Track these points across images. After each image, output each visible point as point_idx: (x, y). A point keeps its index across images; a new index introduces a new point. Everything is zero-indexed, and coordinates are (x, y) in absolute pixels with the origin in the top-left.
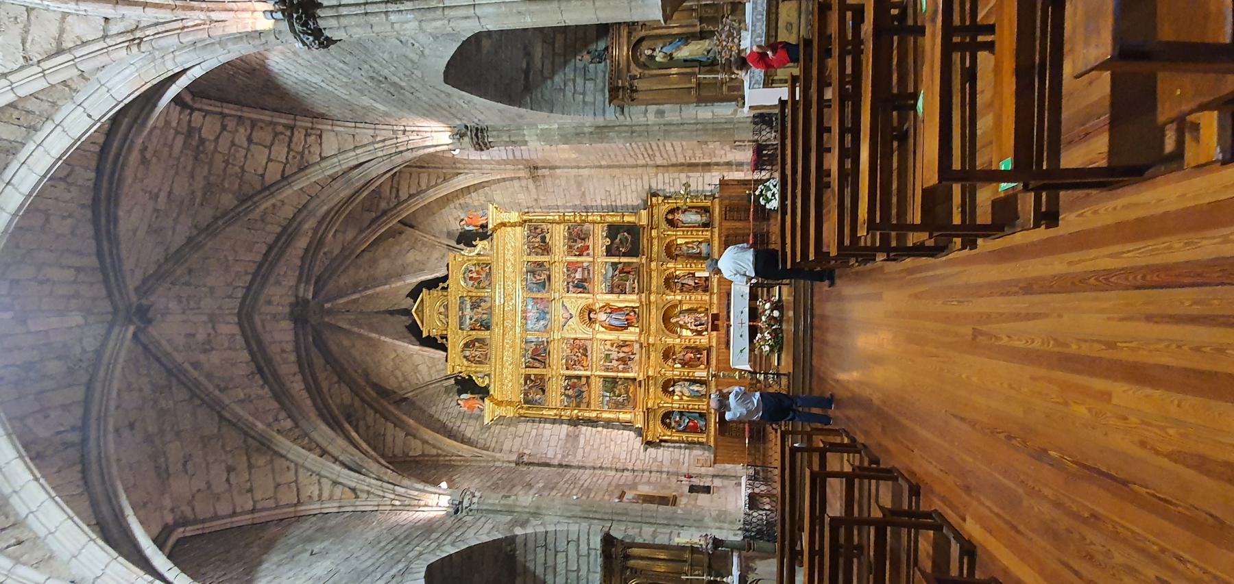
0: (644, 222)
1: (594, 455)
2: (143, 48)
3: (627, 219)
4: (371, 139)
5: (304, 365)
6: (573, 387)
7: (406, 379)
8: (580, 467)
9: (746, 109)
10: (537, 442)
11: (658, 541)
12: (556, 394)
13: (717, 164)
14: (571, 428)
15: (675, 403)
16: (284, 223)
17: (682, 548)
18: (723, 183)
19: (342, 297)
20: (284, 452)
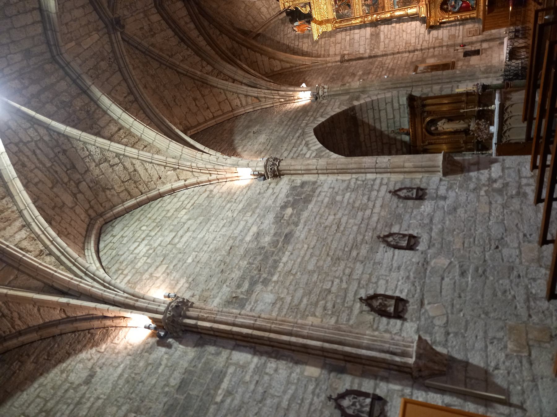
1: (392, 45)
5: (199, 28)
7: (256, 21)
8: (383, 56)
10: (351, 44)
11: (444, 93)
14: (373, 29)
17: (461, 94)
20: (215, 85)
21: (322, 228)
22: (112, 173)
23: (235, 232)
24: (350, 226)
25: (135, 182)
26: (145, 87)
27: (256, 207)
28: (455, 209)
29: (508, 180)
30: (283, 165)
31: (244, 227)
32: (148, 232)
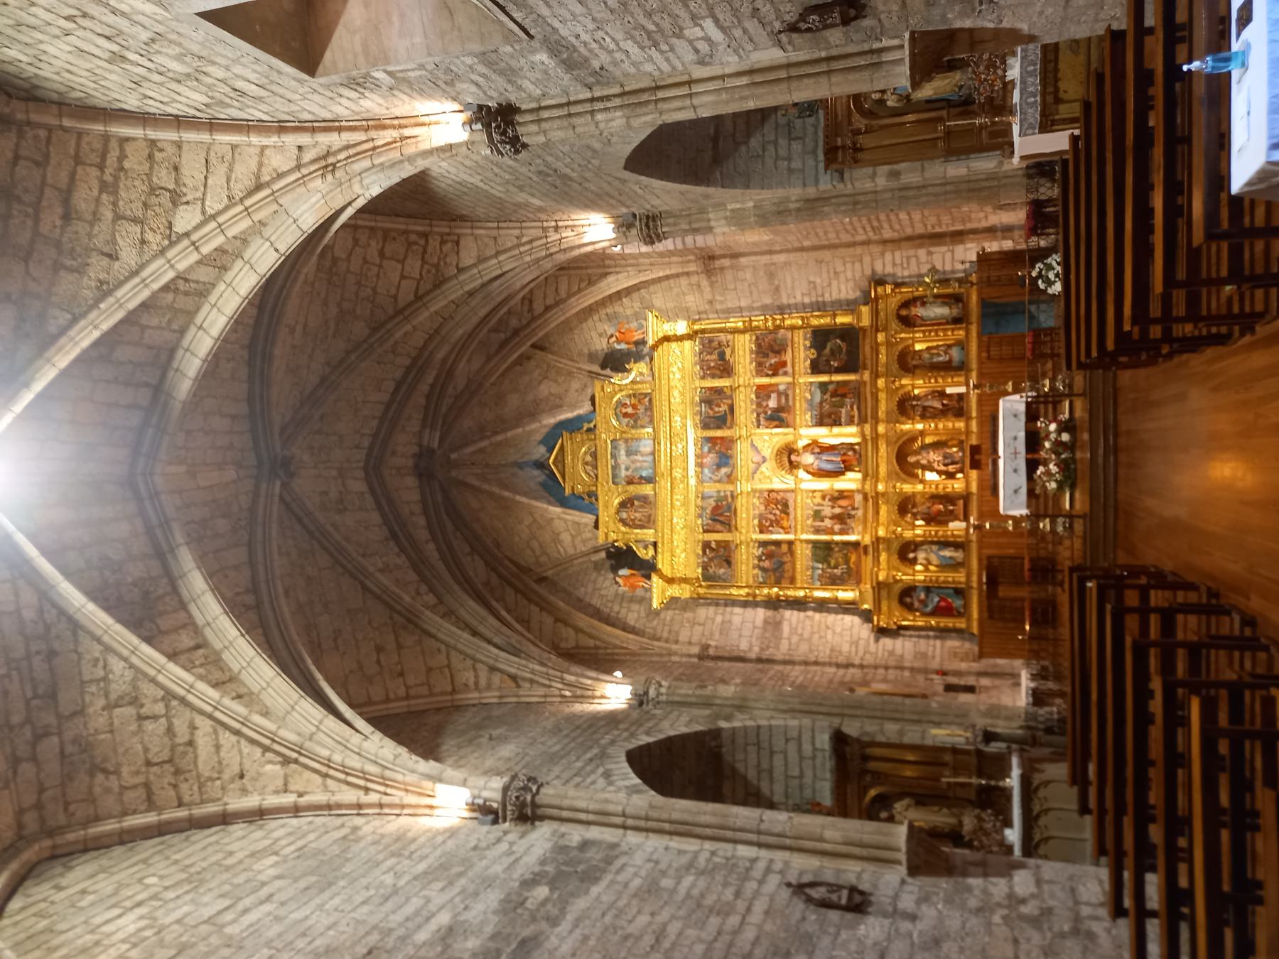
0: (866, 322)
2: (338, 174)
3: (839, 320)
4: (515, 241)
6: (770, 556)
7: (544, 553)
8: (785, 662)
9: (1016, 160)
11: (907, 740)
12: (746, 563)
13: (974, 232)
14: (770, 613)
15: (918, 574)
16: (414, 354)
18: (983, 258)
19: (466, 445)
20: (433, 631)
21: (616, 938)
22: (134, 734)
23: (392, 917)
24: (688, 942)
25: (177, 772)
26: (287, 593)
27: (461, 874)
28: (937, 942)
29: (1051, 903)
30: (548, 795)
31: (417, 913)
32: (160, 889)
